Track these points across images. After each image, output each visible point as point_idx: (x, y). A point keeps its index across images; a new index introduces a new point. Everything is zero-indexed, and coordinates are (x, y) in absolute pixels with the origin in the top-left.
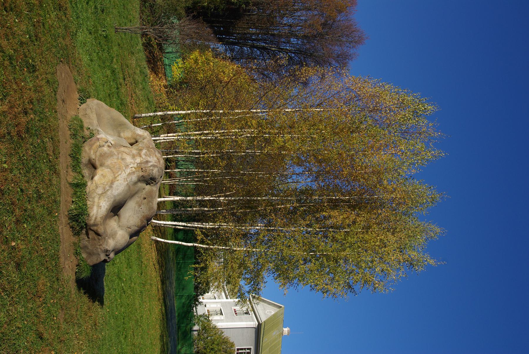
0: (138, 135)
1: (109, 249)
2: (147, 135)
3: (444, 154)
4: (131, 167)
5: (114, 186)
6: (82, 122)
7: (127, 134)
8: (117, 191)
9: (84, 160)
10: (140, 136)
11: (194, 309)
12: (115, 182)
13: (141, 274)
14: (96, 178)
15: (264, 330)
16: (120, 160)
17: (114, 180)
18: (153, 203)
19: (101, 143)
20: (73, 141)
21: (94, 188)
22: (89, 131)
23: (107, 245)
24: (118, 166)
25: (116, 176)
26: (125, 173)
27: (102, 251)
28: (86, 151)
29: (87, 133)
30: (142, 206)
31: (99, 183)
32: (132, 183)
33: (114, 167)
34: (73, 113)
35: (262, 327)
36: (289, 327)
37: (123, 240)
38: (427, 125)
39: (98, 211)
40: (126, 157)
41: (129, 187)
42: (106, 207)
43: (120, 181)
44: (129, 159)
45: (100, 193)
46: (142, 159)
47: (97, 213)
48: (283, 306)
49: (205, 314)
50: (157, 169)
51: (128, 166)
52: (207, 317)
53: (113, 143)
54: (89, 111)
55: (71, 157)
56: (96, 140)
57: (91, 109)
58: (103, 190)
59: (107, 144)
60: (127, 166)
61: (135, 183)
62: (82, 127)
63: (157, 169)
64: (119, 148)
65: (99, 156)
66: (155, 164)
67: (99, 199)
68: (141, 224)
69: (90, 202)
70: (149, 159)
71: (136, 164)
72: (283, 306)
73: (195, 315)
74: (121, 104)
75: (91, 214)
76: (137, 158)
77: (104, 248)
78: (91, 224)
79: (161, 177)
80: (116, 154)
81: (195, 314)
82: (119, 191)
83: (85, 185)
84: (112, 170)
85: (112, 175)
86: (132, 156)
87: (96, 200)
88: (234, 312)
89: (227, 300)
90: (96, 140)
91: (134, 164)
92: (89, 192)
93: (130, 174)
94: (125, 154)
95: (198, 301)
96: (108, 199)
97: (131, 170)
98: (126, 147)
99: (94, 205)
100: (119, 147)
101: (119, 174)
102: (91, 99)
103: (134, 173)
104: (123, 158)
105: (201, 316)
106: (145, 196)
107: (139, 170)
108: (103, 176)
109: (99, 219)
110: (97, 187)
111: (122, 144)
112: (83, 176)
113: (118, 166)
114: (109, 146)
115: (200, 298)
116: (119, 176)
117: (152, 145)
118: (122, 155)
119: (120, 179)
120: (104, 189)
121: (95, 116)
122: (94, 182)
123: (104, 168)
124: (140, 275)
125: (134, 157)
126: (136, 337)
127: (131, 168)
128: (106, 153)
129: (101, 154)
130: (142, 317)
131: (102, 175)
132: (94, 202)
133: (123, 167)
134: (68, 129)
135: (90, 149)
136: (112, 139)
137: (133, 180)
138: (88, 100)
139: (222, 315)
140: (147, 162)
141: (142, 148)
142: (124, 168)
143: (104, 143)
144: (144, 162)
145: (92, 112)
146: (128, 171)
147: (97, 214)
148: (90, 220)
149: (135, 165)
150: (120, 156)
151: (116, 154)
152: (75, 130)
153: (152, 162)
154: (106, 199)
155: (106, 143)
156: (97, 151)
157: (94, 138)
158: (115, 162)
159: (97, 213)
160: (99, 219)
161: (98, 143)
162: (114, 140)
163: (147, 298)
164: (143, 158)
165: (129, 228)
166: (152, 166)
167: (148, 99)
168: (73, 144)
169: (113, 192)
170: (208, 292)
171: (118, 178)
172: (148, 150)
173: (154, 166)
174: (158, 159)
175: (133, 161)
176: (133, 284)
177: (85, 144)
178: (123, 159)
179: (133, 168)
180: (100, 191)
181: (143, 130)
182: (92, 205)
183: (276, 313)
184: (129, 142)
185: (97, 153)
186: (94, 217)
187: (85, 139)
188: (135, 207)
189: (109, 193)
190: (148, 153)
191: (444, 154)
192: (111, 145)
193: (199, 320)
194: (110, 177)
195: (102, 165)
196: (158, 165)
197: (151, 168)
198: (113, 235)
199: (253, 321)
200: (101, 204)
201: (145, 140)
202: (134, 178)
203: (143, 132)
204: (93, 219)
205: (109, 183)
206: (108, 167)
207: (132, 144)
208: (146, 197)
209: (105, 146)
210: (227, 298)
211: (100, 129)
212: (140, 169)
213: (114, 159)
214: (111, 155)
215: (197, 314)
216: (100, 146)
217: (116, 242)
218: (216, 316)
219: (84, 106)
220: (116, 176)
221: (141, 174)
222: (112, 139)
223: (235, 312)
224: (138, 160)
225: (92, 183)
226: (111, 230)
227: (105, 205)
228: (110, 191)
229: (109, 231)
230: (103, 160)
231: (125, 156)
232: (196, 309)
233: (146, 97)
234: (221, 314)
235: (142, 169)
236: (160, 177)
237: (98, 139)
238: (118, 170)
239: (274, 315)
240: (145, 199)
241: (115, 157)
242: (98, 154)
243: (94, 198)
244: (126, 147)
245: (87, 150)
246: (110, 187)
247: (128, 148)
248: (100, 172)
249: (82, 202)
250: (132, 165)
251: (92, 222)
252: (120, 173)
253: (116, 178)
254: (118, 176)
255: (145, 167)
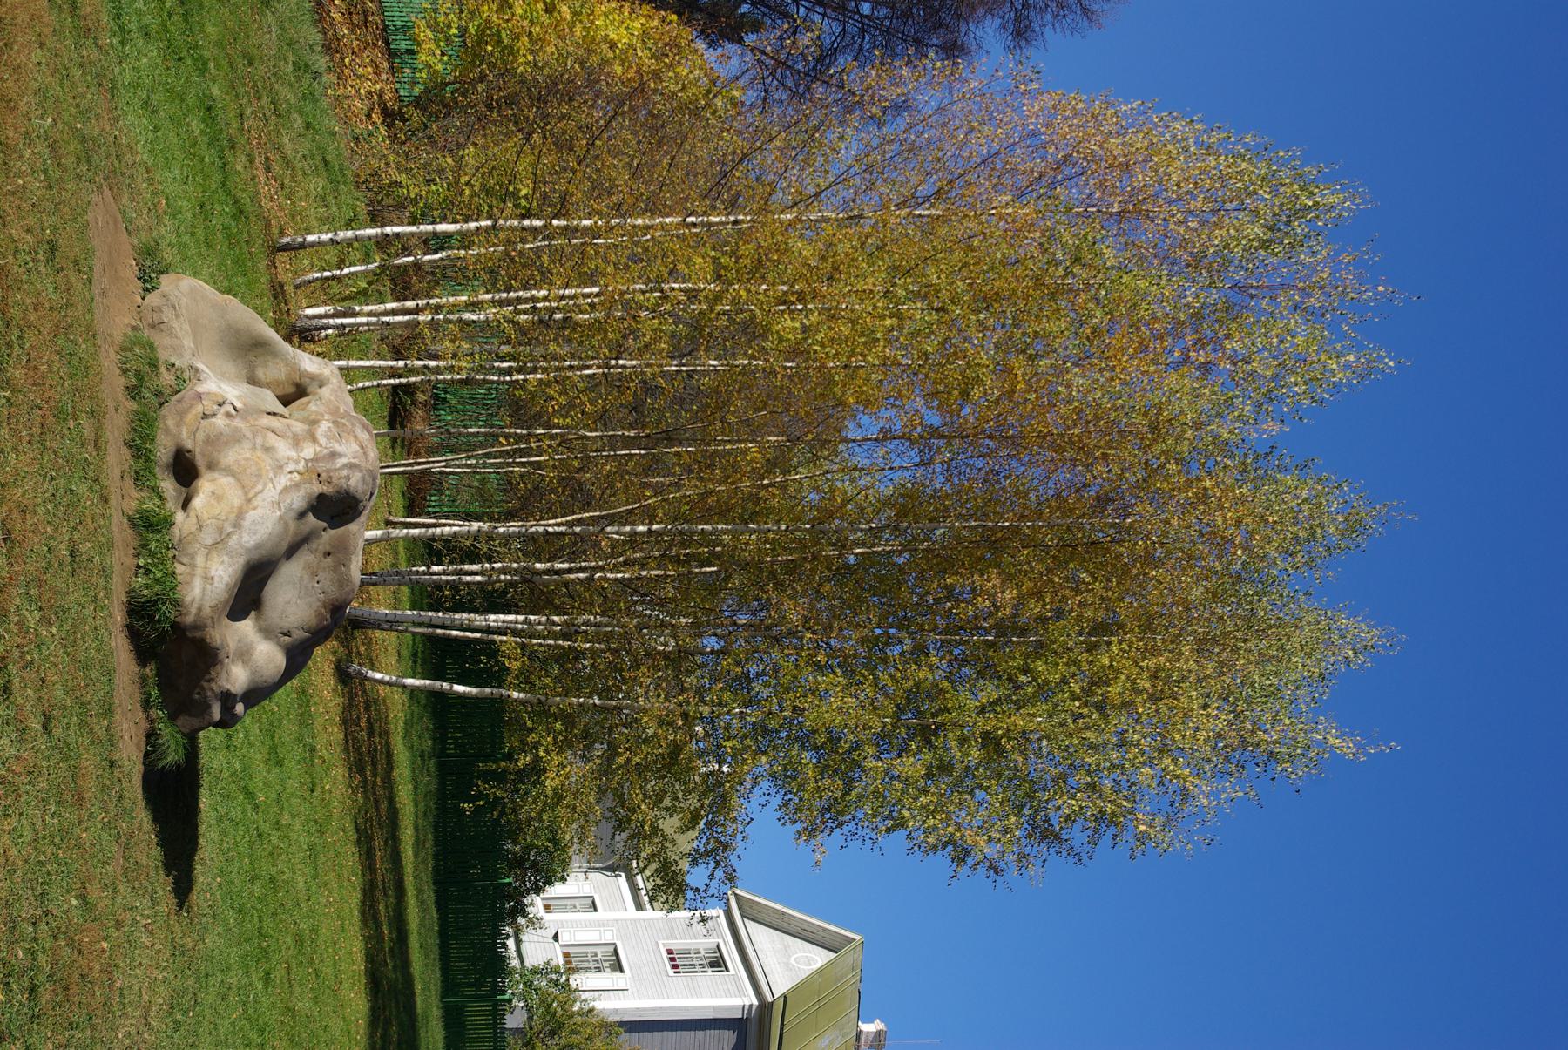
0: (304, 374)
1: (233, 690)
2: (329, 373)
3: (1391, 364)
4: (289, 470)
5: (246, 523)
6: (152, 346)
7: (273, 371)
8: (254, 538)
9: (163, 451)
10: (313, 377)
11: (511, 943)
12: (247, 512)
13: (312, 791)
14: (198, 502)
15: (782, 1029)
16: (259, 453)
17: (245, 507)
18: (349, 567)
19: (207, 404)
20: (133, 405)
21: (193, 529)
22: (173, 371)
23: (228, 680)
24: (253, 468)
25: (251, 494)
26: (274, 487)
27: (216, 696)
28: (167, 431)
29: (167, 378)
30: (322, 576)
31: (206, 515)
32: (293, 514)
33: (245, 470)
34: (127, 321)
35: (774, 1015)
36: (882, 1021)
37: (271, 666)
38: (1333, 259)
39: (204, 590)
40: (276, 445)
41: (286, 524)
42: (226, 579)
43: (259, 511)
44: (283, 449)
45: (209, 541)
46: (318, 449)
47: (204, 595)
48: (857, 937)
49: (553, 963)
50: (360, 475)
51: (281, 467)
52: (557, 978)
53: (238, 405)
54: (167, 315)
55: (131, 447)
56: (194, 399)
57: (174, 307)
58: (217, 536)
59: (223, 410)
60: (279, 468)
61: (301, 515)
62: (154, 364)
63: (360, 475)
64: (256, 420)
65: (203, 442)
66: (353, 461)
67: (207, 560)
68: (317, 625)
69: (183, 568)
70: (338, 448)
71: (303, 463)
72: (857, 937)
73: (514, 969)
74: (235, 217)
75: (188, 599)
76: (305, 445)
77: (220, 687)
78: (186, 626)
79: (372, 494)
80: (249, 435)
81: (515, 963)
82: (258, 536)
83: (169, 522)
84: (239, 480)
85: (240, 492)
86: (290, 441)
87: (200, 560)
88: (666, 961)
89: (641, 914)
90: (194, 399)
91: (297, 462)
92: (180, 541)
93: (286, 489)
94: (272, 435)
95: (525, 915)
96: (232, 557)
97: (291, 479)
98: (274, 414)
99: (194, 575)
100: (255, 416)
101: (256, 490)
102: (172, 276)
103: (297, 486)
104: (267, 445)
105: (534, 971)
106: (328, 548)
107: (311, 479)
108: (215, 495)
109: (207, 611)
110: (201, 526)
111: (263, 408)
112: (161, 498)
113: (253, 468)
114: (228, 415)
115: (532, 904)
116: (259, 497)
117: (346, 404)
118: (264, 437)
119: (260, 504)
120: (220, 530)
121: (187, 327)
122: (192, 514)
123: (216, 475)
124: (307, 794)
125: (296, 442)
126: (297, 990)
127: (291, 472)
128: (221, 434)
129: (208, 437)
130: (314, 930)
131: (213, 493)
132: (193, 566)
133: (267, 471)
134: (118, 371)
135: (178, 424)
136: (236, 393)
137: (294, 506)
138: (164, 279)
139: (622, 971)
140: (333, 455)
141: (319, 417)
142: (271, 475)
143: (216, 407)
144: (324, 457)
145: (177, 316)
146: (284, 481)
147: (202, 599)
148: (185, 614)
149: (301, 466)
150: (259, 440)
151: (249, 435)
152: (138, 374)
153: (345, 456)
154: (226, 559)
155: (220, 405)
156: (197, 429)
157: (187, 394)
158: (247, 459)
159: (204, 595)
160: (207, 611)
161: (200, 408)
162: (240, 396)
163: (332, 876)
164: (321, 446)
165: (285, 635)
166: (345, 466)
167: (326, 163)
168: (136, 413)
169: (244, 539)
170: (563, 879)
171: (255, 502)
172: (334, 422)
173: (351, 466)
174: (362, 447)
175: (293, 454)
176: (286, 817)
177: (165, 410)
178: (267, 449)
179: (296, 474)
180: (208, 537)
181: (319, 360)
182: (189, 574)
183: (830, 963)
184: (279, 394)
185: (197, 435)
186: (195, 605)
187: (161, 397)
188: (301, 577)
189: (233, 541)
190: (335, 431)
191: (1391, 364)
192: (233, 412)
193: (529, 984)
194: (235, 497)
195: (212, 466)
196: (363, 465)
197: (345, 472)
198: (244, 654)
199: (741, 993)
200: (213, 573)
201: (324, 389)
202: (298, 500)
203: (320, 364)
204: (193, 610)
205: (232, 517)
206: (229, 471)
207: (286, 401)
208: (331, 550)
209: (219, 416)
210: (639, 906)
211: (201, 366)
212: (315, 477)
213: (243, 449)
214: (236, 438)
215: (522, 962)
216: (205, 416)
217: (253, 673)
218: (599, 975)
219: (153, 299)
220: (250, 495)
221: (317, 489)
222: (236, 393)
223: (672, 959)
224: (309, 451)
225: (188, 516)
226: (239, 641)
227: (222, 573)
228: (235, 537)
229: (232, 645)
230: (215, 454)
231: (273, 440)
232: (518, 942)
233: (319, 158)
234: (618, 966)
235: (319, 475)
236: (367, 497)
237: (199, 396)
238: (255, 479)
239: (820, 971)
240: (329, 554)
241: (247, 445)
242: (200, 436)
243: (192, 557)
244: (274, 414)
245: (172, 427)
246: (235, 526)
247: (281, 419)
248: (206, 486)
249: (161, 567)
250: (291, 467)
251: (189, 619)
252: (260, 487)
253: (249, 501)
254: (256, 495)
255: (328, 471)
